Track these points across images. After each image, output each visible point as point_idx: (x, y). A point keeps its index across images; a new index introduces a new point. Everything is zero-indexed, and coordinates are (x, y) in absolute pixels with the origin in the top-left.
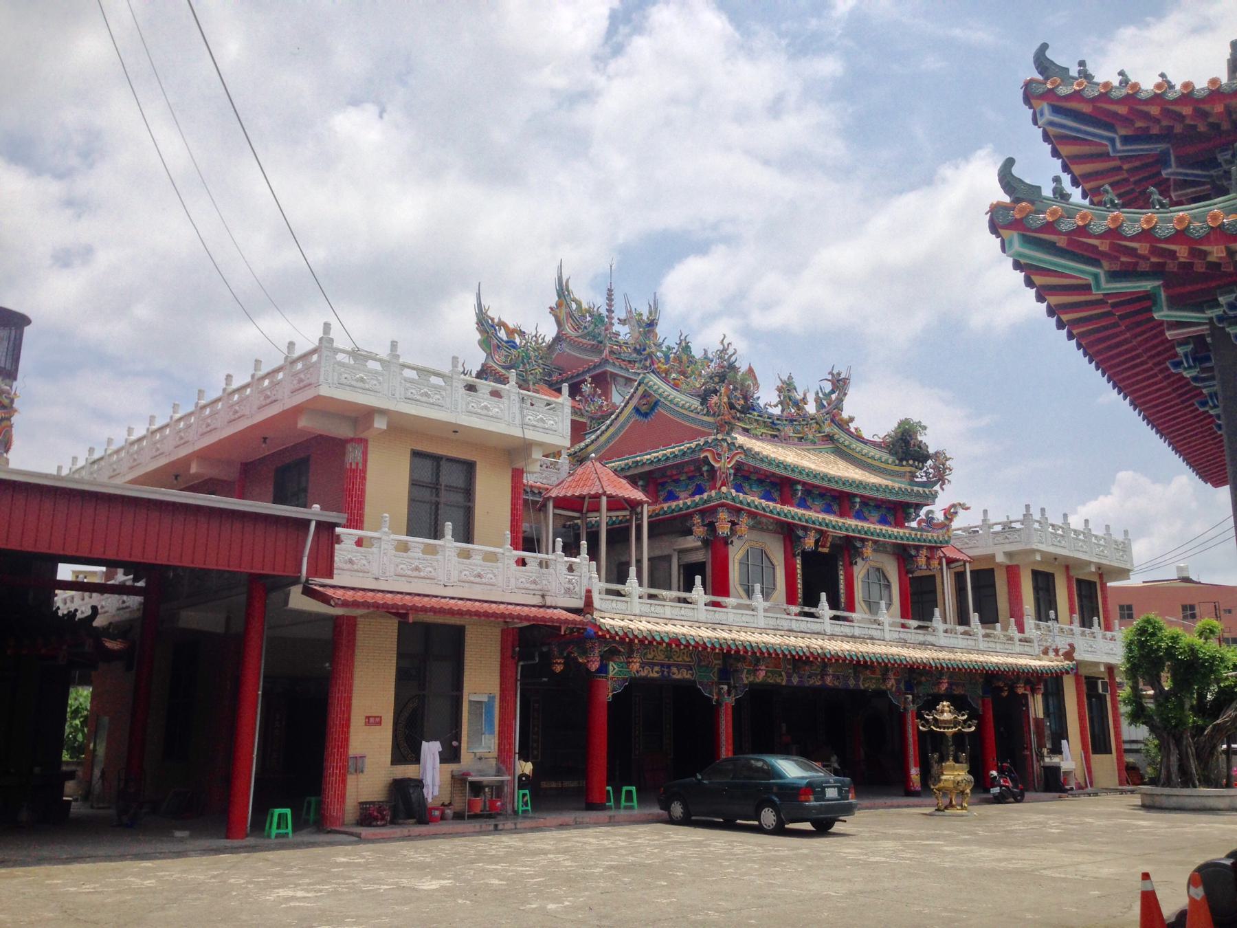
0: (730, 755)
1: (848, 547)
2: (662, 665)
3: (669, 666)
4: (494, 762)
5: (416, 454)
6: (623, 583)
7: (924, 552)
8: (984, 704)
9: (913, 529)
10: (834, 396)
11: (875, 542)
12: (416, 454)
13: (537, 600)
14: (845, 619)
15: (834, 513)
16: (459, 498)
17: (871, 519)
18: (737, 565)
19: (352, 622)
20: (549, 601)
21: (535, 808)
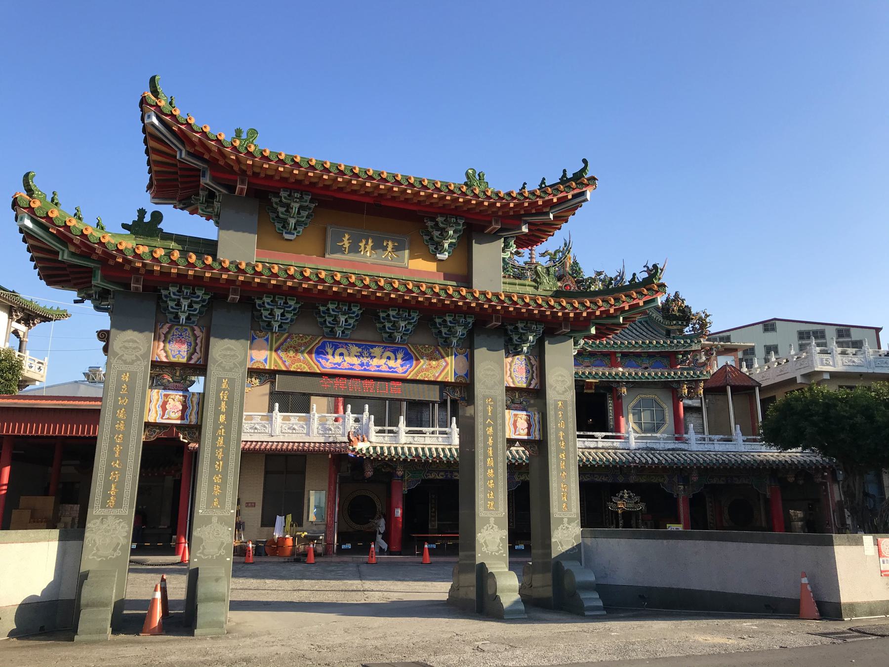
2: (446, 472)
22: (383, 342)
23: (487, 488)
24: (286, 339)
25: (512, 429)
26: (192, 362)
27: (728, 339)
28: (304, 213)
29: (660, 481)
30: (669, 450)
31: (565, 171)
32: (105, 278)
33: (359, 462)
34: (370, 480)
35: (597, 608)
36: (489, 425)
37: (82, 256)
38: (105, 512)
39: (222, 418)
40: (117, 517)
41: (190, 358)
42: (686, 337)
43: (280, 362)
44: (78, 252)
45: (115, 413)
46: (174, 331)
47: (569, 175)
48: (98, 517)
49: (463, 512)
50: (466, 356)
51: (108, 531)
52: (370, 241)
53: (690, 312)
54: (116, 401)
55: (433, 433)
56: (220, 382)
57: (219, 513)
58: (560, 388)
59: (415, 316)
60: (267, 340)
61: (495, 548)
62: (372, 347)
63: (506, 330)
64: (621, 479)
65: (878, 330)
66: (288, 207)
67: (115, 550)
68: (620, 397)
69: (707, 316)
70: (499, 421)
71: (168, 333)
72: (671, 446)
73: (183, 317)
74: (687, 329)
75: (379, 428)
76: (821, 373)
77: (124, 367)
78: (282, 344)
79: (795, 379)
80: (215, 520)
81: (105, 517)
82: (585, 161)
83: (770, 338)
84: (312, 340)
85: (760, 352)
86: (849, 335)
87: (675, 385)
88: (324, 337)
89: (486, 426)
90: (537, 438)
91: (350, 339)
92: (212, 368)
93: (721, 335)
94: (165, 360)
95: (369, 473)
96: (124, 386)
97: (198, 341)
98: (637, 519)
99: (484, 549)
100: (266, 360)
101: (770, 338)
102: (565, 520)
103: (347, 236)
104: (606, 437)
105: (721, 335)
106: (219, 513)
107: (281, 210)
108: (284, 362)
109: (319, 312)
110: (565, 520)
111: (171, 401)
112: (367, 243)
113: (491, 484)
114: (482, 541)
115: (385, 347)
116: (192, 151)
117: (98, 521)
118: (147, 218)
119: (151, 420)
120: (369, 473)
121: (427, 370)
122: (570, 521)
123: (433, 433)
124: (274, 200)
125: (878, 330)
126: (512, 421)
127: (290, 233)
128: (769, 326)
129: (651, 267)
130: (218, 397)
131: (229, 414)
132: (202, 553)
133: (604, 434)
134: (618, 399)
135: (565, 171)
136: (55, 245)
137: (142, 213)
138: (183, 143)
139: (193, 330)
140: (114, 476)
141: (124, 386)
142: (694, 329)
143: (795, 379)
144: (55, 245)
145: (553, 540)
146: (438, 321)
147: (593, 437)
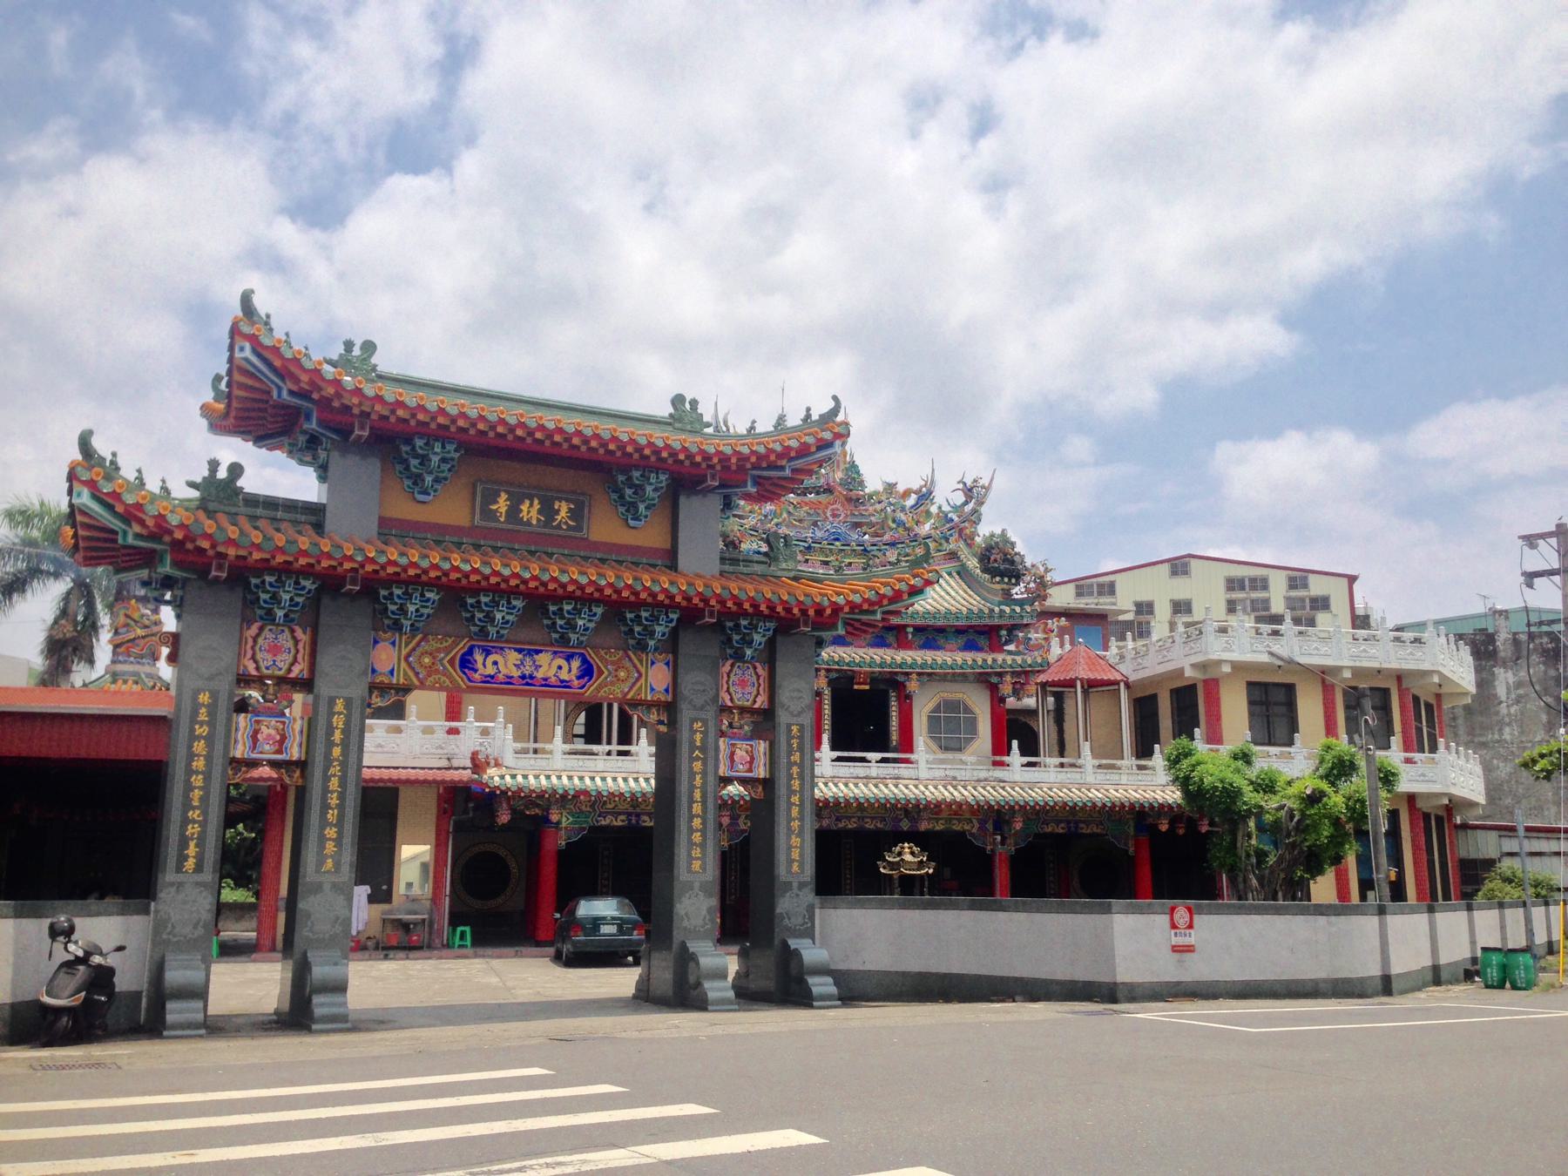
0: (254, 924)
1: (891, 684)
2: (629, 814)
3: (638, 815)
4: (428, 903)
5: (1250, 684)
6: (629, 743)
7: (1008, 678)
8: (1137, 845)
9: (1010, 653)
10: (968, 508)
11: (919, 674)
12: (1250, 684)
13: (444, 763)
14: (1112, 767)
15: (889, 646)
16: (1283, 709)
17: (1347, 674)
18: (925, 719)
19: (397, 790)
20: (455, 763)
21: (475, 943)
22: (552, 645)
23: (691, 844)
24: (418, 644)
25: (728, 763)
26: (292, 675)
27: (1110, 589)
28: (445, 467)
29: (967, 827)
30: (979, 781)
31: (808, 409)
32: (175, 564)
33: (488, 800)
34: (506, 828)
35: (829, 997)
36: (698, 758)
37: (152, 537)
38: (180, 877)
39: (337, 751)
40: (197, 884)
41: (289, 670)
42: (1017, 602)
43: (411, 674)
44: (144, 532)
45: (190, 747)
46: (266, 632)
47: (815, 417)
48: (172, 884)
49: (657, 877)
50: (667, 664)
51: (185, 902)
52: (536, 502)
53: (1023, 562)
54: (192, 730)
55: (609, 753)
56: (332, 701)
57: (333, 879)
58: (795, 707)
59: (599, 610)
60: (393, 643)
61: (700, 922)
62: (538, 652)
63: (723, 628)
64: (905, 825)
65: (1352, 579)
66: (424, 460)
67: (195, 927)
68: (909, 697)
69: (1047, 571)
70: (711, 753)
71: (258, 635)
72: (983, 775)
73: (280, 613)
74: (1016, 589)
75: (519, 746)
76: (1219, 662)
77: (200, 683)
78: (414, 649)
79: (1182, 670)
80: (327, 887)
81: (180, 885)
82: (835, 398)
83: (1181, 589)
84: (455, 644)
85: (1163, 612)
86: (1305, 586)
87: (994, 680)
88: (471, 639)
89: (692, 759)
90: (762, 776)
91: (507, 641)
92: (323, 687)
93: (1101, 579)
94: (254, 673)
95: (504, 817)
96: (203, 710)
97: (301, 646)
98: (922, 886)
99: (686, 923)
100: (392, 672)
101: (1181, 589)
102: (795, 885)
103: (504, 496)
104: (884, 760)
105: (1101, 579)
106: (333, 879)
107: (414, 462)
108: (417, 674)
109: (464, 605)
110: (795, 885)
111: (263, 728)
112: (531, 505)
113: (697, 837)
114: (682, 912)
115: (555, 653)
116: (295, 388)
117: (173, 890)
118: (222, 474)
119: (238, 755)
120: (504, 817)
121: (612, 683)
122: (802, 885)
123: (609, 753)
124: (405, 448)
125: (1352, 579)
126: (728, 751)
127: (426, 493)
128: (1179, 566)
129: (969, 484)
130: (330, 724)
131: (345, 744)
132: (311, 930)
133: (879, 756)
134: (906, 700)
135: (808, 409)
136: (116, 524)
137: (214, 465)
138: (282, 378)
139: (292, 631)
140: (193, 830)
141: (203, 710)
142: (1027, 590)
143: (1182, 670)
144: (116, 524)
145: (778, 911)
146: (629, 616)
147: (863, 760)
